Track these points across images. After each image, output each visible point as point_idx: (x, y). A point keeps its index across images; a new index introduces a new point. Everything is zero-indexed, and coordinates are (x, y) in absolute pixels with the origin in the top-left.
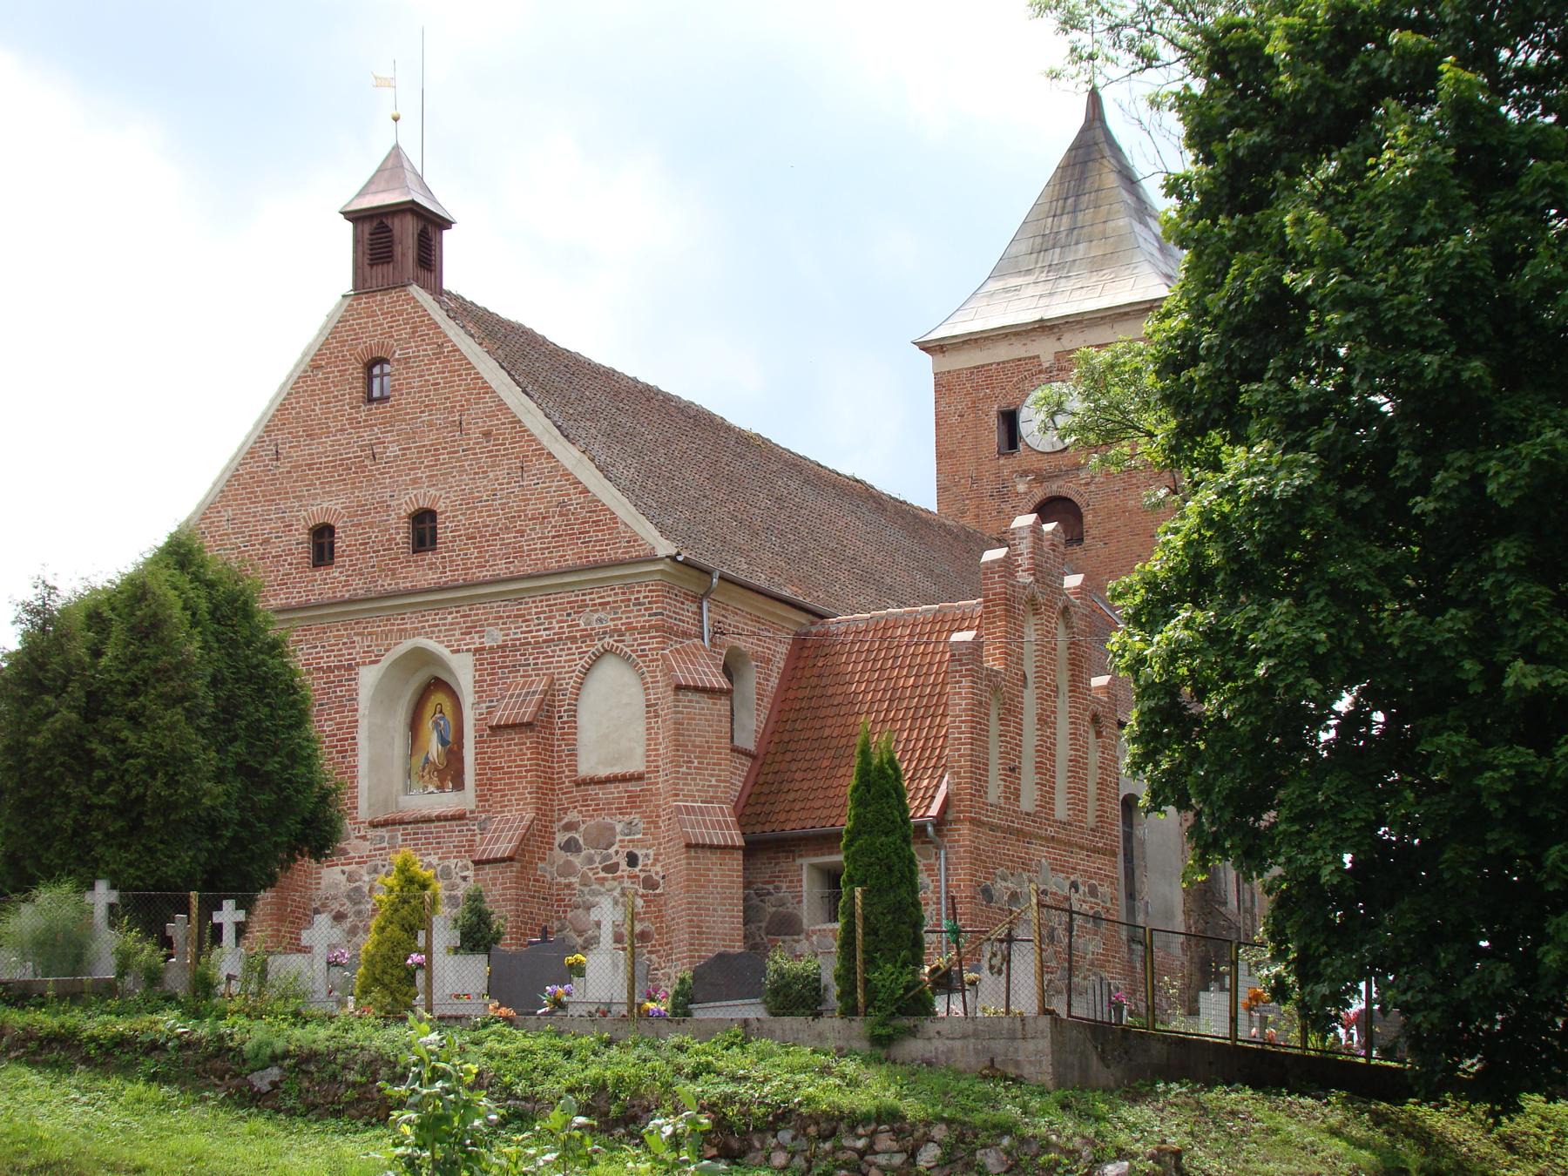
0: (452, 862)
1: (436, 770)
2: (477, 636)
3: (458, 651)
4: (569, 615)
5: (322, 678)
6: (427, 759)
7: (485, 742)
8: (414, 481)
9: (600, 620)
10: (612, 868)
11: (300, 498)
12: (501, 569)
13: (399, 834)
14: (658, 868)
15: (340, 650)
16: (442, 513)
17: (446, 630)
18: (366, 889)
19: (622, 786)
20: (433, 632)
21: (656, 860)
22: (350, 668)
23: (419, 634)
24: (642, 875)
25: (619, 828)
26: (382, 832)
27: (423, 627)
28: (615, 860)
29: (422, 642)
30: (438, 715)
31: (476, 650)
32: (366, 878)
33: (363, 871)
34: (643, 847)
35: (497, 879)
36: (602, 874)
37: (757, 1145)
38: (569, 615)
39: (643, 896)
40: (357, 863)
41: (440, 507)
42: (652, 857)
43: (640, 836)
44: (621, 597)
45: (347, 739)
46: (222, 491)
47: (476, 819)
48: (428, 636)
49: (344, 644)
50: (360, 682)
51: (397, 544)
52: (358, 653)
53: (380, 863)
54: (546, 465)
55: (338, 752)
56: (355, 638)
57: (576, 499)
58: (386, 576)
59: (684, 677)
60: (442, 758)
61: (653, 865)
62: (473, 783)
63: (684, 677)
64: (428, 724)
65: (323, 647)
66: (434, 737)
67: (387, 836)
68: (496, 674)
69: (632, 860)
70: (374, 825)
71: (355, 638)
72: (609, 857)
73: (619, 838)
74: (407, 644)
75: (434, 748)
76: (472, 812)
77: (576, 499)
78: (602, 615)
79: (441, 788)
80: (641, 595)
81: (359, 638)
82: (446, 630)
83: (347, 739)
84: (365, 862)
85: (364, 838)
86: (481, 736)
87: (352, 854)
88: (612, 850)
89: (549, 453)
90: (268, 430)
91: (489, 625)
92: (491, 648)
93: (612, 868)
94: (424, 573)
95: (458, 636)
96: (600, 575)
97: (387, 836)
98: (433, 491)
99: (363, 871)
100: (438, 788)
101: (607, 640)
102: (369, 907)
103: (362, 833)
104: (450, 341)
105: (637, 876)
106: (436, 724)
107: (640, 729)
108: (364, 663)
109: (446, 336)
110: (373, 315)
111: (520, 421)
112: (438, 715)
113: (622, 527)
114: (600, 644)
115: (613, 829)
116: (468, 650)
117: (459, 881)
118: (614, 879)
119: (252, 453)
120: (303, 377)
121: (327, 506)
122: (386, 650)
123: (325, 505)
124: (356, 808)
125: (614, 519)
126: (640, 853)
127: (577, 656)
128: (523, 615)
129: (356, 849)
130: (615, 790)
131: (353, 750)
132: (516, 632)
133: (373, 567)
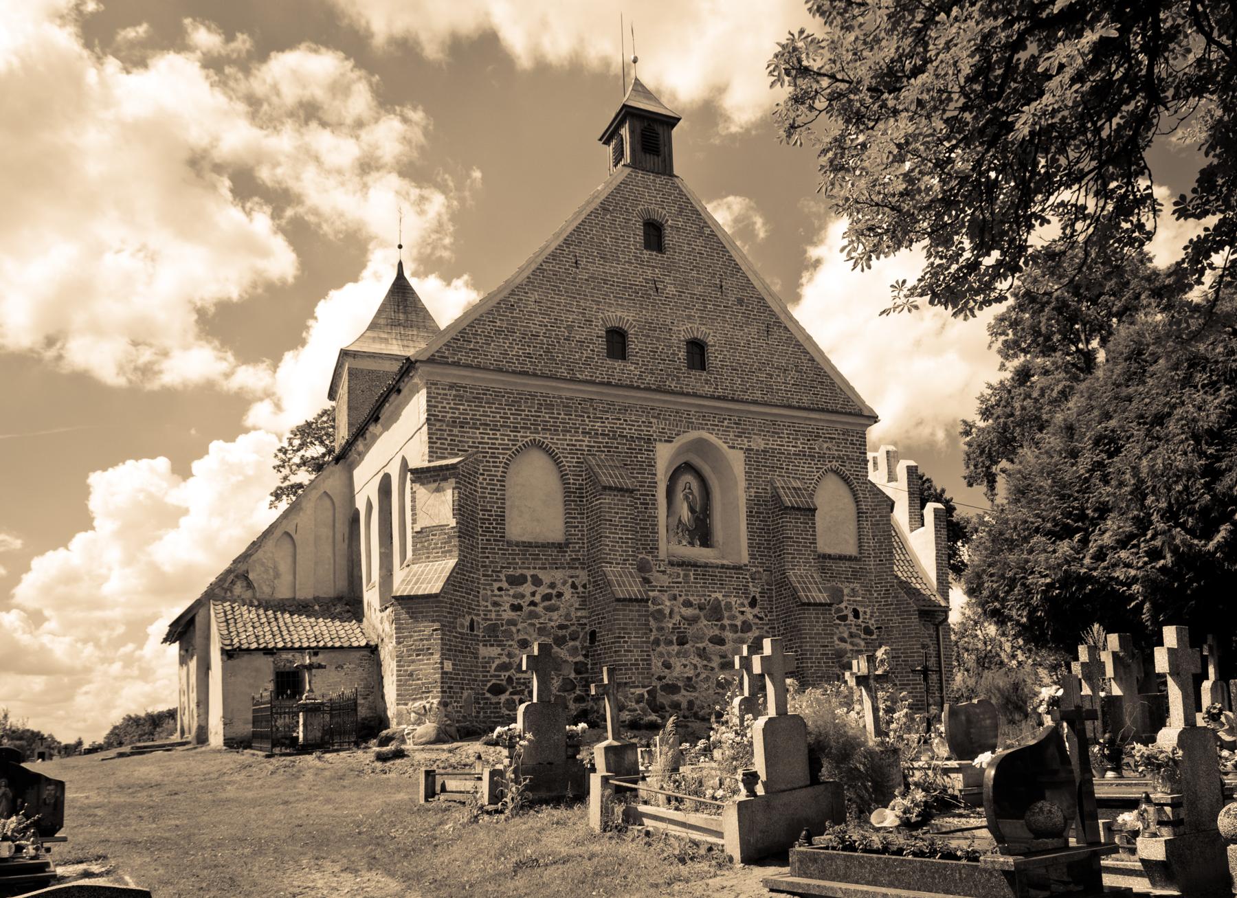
0: (733, 600)
1: (688, 530)
2: (746, 440)
3: (734, 448)
4: (809, 440)
5: (625, 444)
6: (680, 521)
7: (753, 516)
8: (689, 317)
9: (829, 449)
10: (844, 618)
11: (598, 303)
12: (758, 395)
13: (691, 574)
14: (873, 621)
15: (640, 426)
16: (712, 346)
17: (723, 431)
18: (667, 612)
19: (847, 564)
20: (714, 430)
21: (872, 616)
22: (649, 441)
23: (703, 429)
24: (863, 625)
25: (846, 591)
26: (679, 570)
27: (707, 424)
28: (845, 612)
29: (705, 435)
30: (687, 491)
31: (747, 449)
32: (668, 603)
33: (665, 597)
34: (862, 606)
35: (819, 618)
36: (837, 622)
37: (1168, 809)
38: (809, 440)
39: (864, 639)
40: (659, 591)
41: (710, 340)
42: (868, 613)
43: (860, 599)
44: (842, 437)
45: (648, 495)
46: (529, 278)
47: (749, 570)
48: (710, 431)
49: (643, 422)
50: (657, 454)
51: (679, 359)
52: (655, 432)
53: (677, 593)
54: (785, 336)
55: (641, 504)
56: (652, 420)
57: (804, 359)
58: (673, 380)
59: (790, 501)
60: (692, 521)
61: (870, 619)
62: (746, 545)
63: (790, 501)
64: (680, 496)
65: (625, 421)
66: (685, 506)
67: (682, 573)
68: (760, 470)
69: (856, 614)
70: (671, 564)
71: (652, 420)
72: (841, 610)
73: (846, 598)
74: (693, 435)
75: (685, 513)
76: (746, 565)
77: (804, 359)
78: (830, 445)
79: (692, 544)
80: (855, 439)
81: (655, 421)
82: (723, 431)
83: (648, 495)
84: (666, 591)
85: (664, 572)
86: (751, 512)
87: (654, 584)
88: (843, 605)
89: (785, 327)
90: (567, 242)
91: (755, 434)
92: (757, 450)
93: (844, 618)
94: (695, 381)
95: (732, 436)
96: (834, 417)
97: (682, 573)
98: (703, 328)
99: (665, 597)
100: (689, 543)
101: (834, 463)
102: (670, 625)
103: (662, 569)
104: (709, 227)
105: (860, 626)
106: (686, 498)
107: (852, 527)
108: (660, 440)
109: (705, 223)
110: (647, 187)
111: (763, 299)
112: (687, 491)
113: (838, 390)
114: (829, 464)
115: (842, 591)
116: (741, 449)
117: (737, 614)
118: (845, 625)
119: (553, 256)
120: (594, 212)
121: (622, 315)
122: (677, 435)
123: (619, 314)
124: (657, 549)
125: (833, 384)
126: (861, 610)
127: (815, 470)
128: (778, 433)
129: (657, 580)
130: (844, 566)
131: (654, 504)
132: (773, 444)
133: (661, 370)
